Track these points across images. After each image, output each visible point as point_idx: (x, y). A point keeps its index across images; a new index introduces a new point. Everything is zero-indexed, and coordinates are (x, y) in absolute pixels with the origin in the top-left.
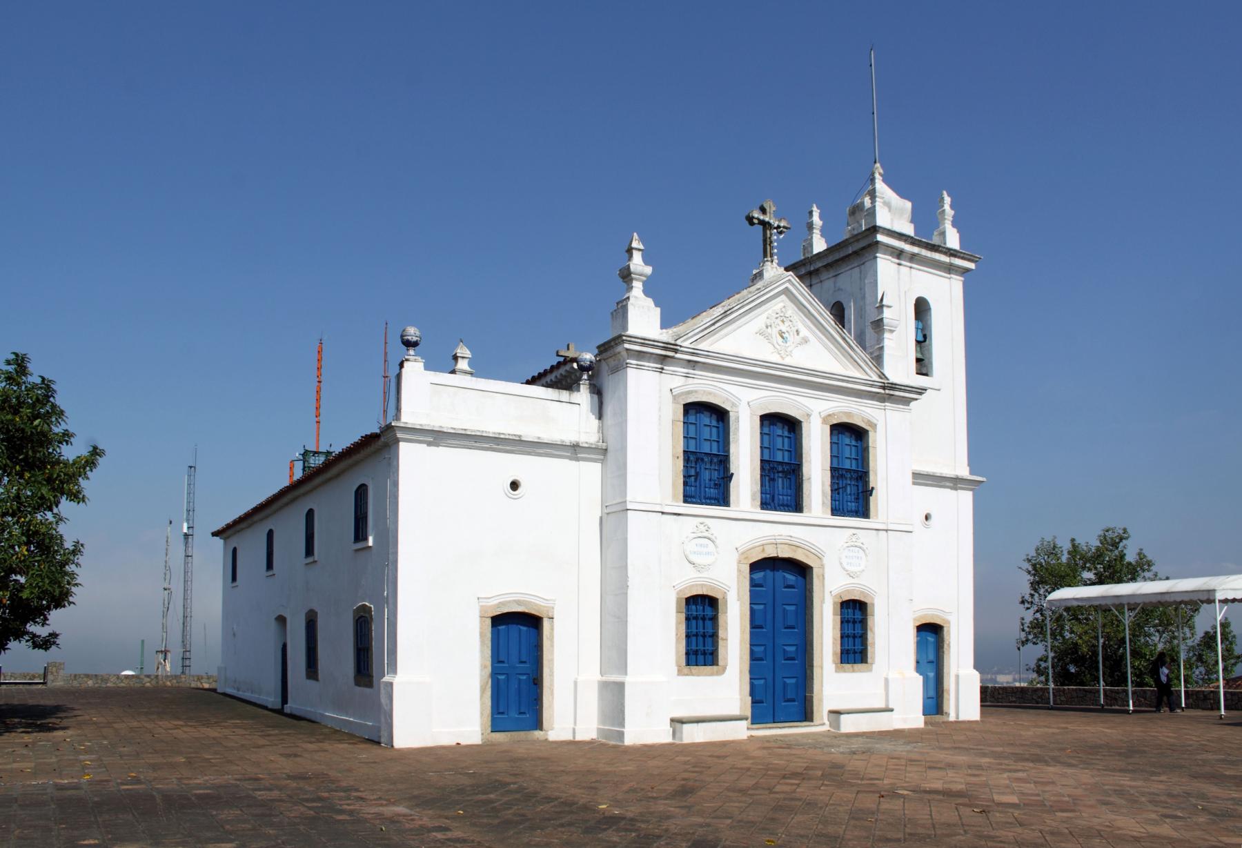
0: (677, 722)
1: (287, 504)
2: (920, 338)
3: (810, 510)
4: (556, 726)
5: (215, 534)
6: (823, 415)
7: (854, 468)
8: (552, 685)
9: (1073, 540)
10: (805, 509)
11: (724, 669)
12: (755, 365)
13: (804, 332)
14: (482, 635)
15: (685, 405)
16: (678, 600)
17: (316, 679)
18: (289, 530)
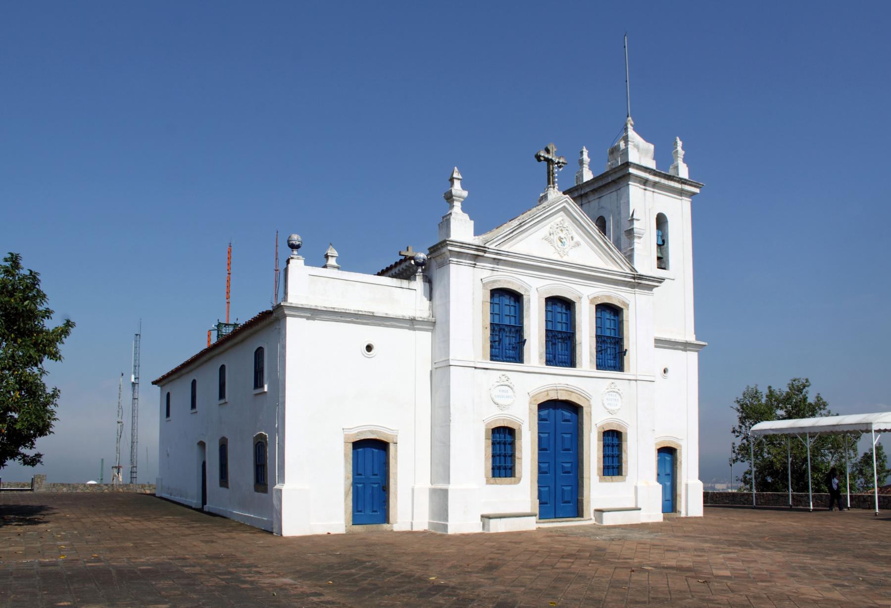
0: (486, 518)
1: (206, 362)
2: (660, 243)
3: (581, 366)
4: (399, 520)
5: (154, 383)
6: (590, 297)
7: (613, 335)
8: (396, 491)
9: (770, 387)
10: (577, 365)
11: (520, 479)
12: (542, 262)
13: (577, 238)
14: (346, 455)
15: (492, 291)
16: (487, 430)
17: (227, 487)
18: (207, 380)
